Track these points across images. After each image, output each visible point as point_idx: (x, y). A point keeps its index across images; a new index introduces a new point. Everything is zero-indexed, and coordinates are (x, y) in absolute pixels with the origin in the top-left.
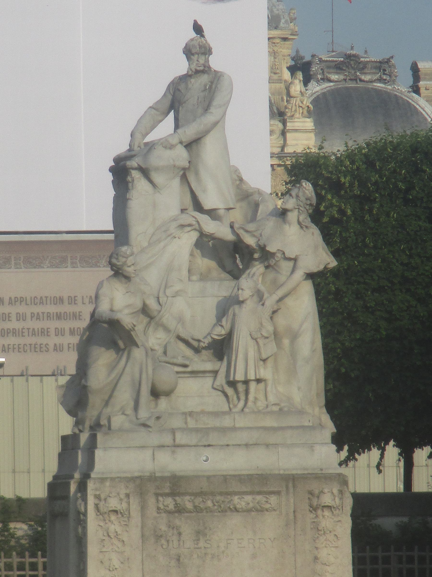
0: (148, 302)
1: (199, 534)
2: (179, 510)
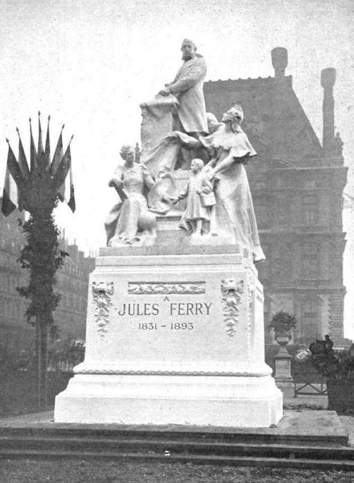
0: (146, 179)
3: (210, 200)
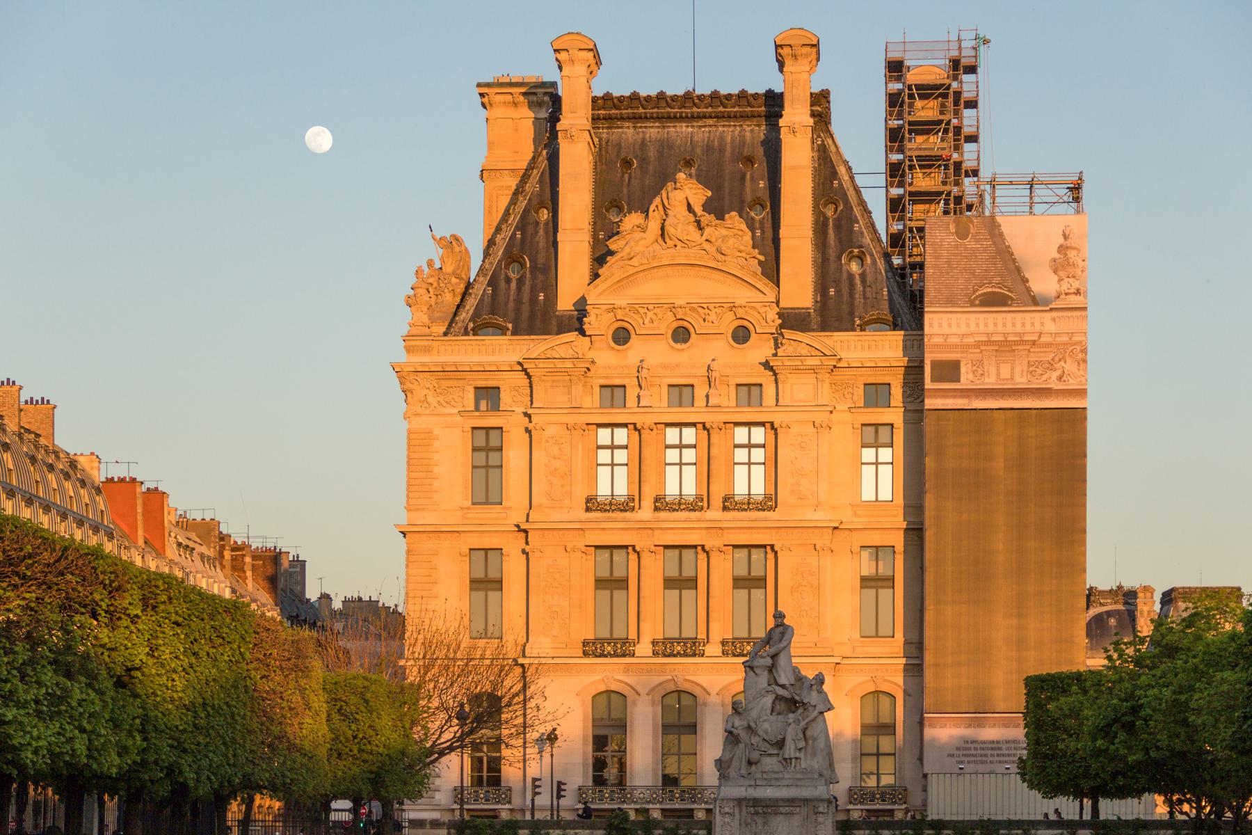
1: (765, 823)
2: (756, 813)
3: (802, 744)
